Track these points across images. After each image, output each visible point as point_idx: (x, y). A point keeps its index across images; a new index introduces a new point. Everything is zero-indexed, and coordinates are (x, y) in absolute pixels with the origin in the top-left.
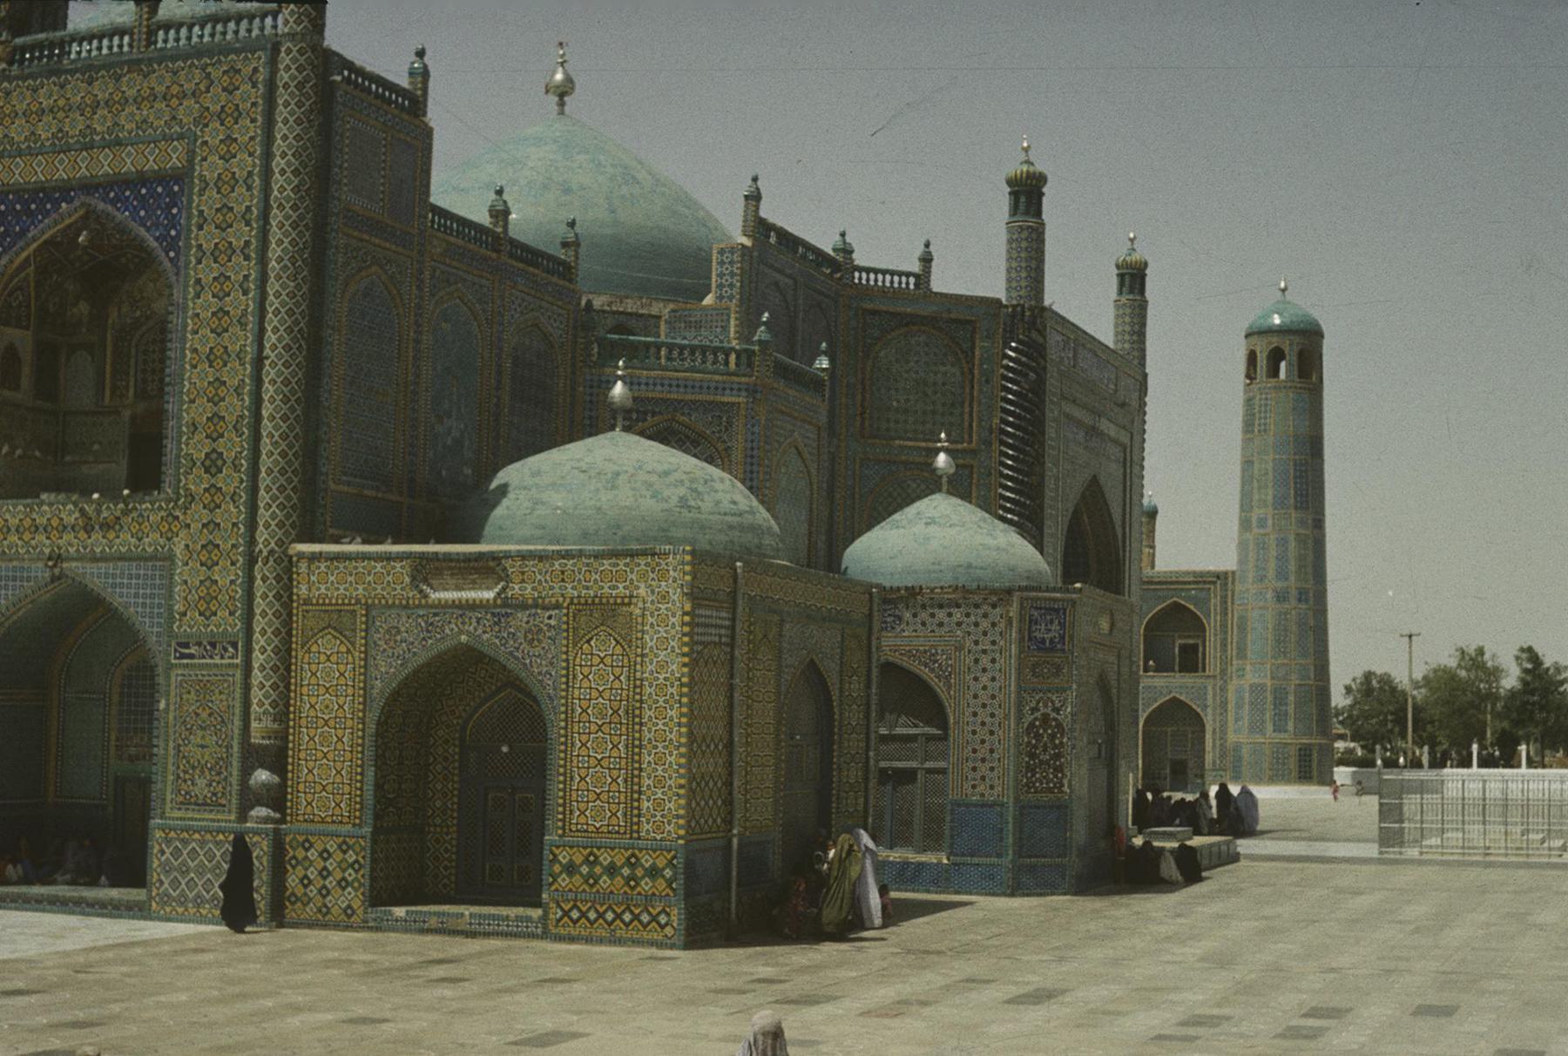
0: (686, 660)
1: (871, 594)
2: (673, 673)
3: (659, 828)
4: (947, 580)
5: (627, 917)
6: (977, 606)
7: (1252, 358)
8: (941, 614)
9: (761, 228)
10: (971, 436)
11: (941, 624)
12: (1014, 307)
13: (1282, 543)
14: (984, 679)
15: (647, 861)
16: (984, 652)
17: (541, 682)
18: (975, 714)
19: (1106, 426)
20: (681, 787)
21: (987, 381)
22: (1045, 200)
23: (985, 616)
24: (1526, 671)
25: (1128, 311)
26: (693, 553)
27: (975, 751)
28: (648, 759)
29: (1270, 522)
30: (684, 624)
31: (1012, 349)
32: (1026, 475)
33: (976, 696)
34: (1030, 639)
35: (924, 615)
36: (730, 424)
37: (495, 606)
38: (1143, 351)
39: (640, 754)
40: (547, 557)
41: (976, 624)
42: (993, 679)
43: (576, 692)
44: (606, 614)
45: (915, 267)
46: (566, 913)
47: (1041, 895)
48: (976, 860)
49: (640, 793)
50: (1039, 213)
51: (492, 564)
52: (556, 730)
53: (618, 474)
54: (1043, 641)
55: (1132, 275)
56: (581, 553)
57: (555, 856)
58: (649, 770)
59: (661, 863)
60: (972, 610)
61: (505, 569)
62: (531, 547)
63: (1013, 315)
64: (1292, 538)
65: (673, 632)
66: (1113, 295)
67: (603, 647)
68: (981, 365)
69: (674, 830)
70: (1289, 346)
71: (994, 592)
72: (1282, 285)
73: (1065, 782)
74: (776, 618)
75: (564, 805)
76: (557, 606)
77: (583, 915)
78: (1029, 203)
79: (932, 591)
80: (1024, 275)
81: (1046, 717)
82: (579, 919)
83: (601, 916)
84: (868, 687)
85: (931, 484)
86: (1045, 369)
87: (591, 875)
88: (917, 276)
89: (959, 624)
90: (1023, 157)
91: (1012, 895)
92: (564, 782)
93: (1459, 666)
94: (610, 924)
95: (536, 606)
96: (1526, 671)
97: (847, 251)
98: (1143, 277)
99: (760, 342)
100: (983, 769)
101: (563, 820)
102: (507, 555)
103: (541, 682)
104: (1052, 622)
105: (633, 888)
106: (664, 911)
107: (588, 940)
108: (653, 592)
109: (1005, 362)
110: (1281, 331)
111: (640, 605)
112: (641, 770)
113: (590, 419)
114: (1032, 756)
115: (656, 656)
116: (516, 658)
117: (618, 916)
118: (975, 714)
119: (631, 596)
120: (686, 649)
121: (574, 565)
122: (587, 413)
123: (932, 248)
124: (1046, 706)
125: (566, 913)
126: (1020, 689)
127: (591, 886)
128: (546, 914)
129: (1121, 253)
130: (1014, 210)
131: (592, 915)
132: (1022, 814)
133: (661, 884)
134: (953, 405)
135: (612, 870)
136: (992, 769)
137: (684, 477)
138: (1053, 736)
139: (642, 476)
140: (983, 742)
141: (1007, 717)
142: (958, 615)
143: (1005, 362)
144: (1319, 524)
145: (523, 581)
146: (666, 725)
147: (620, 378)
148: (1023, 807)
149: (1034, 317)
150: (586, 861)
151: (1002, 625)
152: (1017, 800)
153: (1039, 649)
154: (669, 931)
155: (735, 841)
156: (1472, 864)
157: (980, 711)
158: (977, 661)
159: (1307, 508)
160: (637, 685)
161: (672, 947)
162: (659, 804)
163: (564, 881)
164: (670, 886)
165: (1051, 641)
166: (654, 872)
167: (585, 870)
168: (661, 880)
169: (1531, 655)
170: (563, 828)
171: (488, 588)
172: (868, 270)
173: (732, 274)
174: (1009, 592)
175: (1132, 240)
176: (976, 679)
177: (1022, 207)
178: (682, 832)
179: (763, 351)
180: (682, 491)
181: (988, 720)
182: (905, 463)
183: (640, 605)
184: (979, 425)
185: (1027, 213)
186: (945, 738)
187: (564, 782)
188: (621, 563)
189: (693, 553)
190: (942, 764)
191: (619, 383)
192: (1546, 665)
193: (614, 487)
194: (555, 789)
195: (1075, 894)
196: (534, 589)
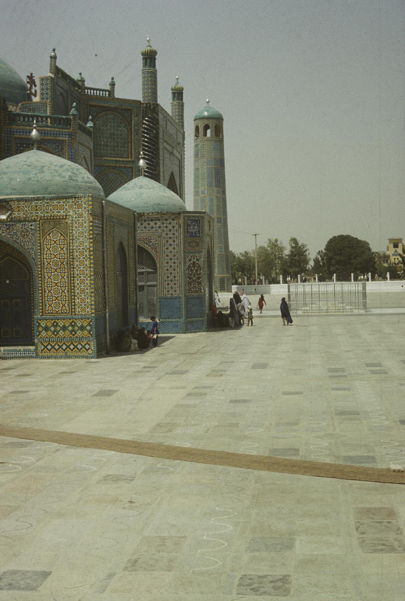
0: (91, 241)
1: (134, 215)
2: (86, 246)
3: (83, 310)
4: (151, 210)
5: (72, 347)
6: (166, 220)
7: (197, 129)
8: (152, 224)
9: (58, 71)
10: (132, 156)
11: (152, 228)
12: (147, 104)
13: (211, 200)
14: (171, 249)
15: (79, 324)
16: (170, 238)
17: (29, 252)
18: (167, 263)
19: (175, 152)
20: (92, 292)
21: (137, 134)
22: (156, 61)
23: (170, 223)
24: (293, 247)
25: (177, 107)
26: (92, 196)
27: (168, 277)
28: (77, 282)
29: (206, 193)
30: (89, 226)
31: (146, 120)
32: (154, 170)
33: (167, 256)
34: (187, 232)
35: (145, 224)
36: (62, 148)
37: (7, 221)
38: (183, 123)
39: (74, 280)
40: (29, 200)
41: (167, 227)
42: (174, 248)
43: (45, 256)
44: (56, 223)
45: (108, 88)
46: (45, 347)
47: (195, 332)
48: (170, 320)
49: (74, 296)
50: (154, 66)
51: (4, 204)
52: (36, 271)
53: (43, 167)
54: (192, 233)
55: (178, 93)
56: (44, 198)
57: (39, 324)
58: (78, 286)
59: (85, 324)
60: (165, 222)
61: (11, 206)
62: (21, 196)
63: (146, 107)
64: (215, 198)
65: (85, 230)
66: (171, 101)
67: (55, 237)
68: (134, 127)
69: (89, 311)
70: (211, 123)
71: (173, 214)
72: (207, 100)
73: (202, 288)
74: (112, 224)
75: (42, 303)
76: (35, 221)
77: (53, 347)
78: (151, 62)
79: (148, 214)
80: (150, 91)
81: (194, 264)
82: (51, 349)
83: (60, 347)
84: (135, 252)
85: (138, 172)
86: (159, 128)
87: (55, 331)
88: (109, 91)
89: (159, 227)
90: (148, 44)
91: (185, 333)
92: (42, 293)
93: (268, 246)
94: (64, 350)
95: (25, 221)
96: (293, 247)
97: (83, 81)
98: (182, 93)
99: (73, 115)
100: (172, 284)
101: (42, 309)
102: (12, 200)
103: (29, 252)
104: (195, 225)
105: (73, 335)
106: (87, 343)
107: (56, 357)
108: (76, 213)
109: (144, 126)
110: (208, 118)
111: (71, 218)
112: (74, 287)
113: (25, 145)
114: (190, 278)
115: (79, 239)
116: (18, 243)
117: (68, 347)
118: (167, 263)
119: (66, 215)
120: (91, 236)
121: (41, 203)
122: (6, 145)
123: (114, 80)
124: (194, 258)
125: (45, 347)
126: (185, 252)
127: (56, 335)
128: (37, 349)
129: (173, 84)
130: (145, 64)
131: (57, 347)
132: (187, 301)
133: (86, 332)
134: (124, 143)
135: (64, 328)
136: (175, 284)
137: (69, 168)
138: (197, 270)
139: (53, 167)
140: (171, 273)
141: (180, 263)
142: (159, 223)
143: (144, 126)
144: (224, 193)
145: (19, 211)
146: (84, 269)
147: (35, 128)
148: (187, 298)
149: (154, 108)
150: (53, 325)
151: (177, 227)
152: (185, 296)
153: (191, 236)
154: (90, 351)
155: (107, 314)
156: (314, 316)
157: (169, 261)
158: (167, 241)
159: (220, 187)
160: (71, 252)
161: (92, 358)
162: (83, 300)
163: (44, 333)
164: (89, 333)
165: (195, 233)
166: (82, 328)
167: (52, 329)
168: (85, 331)
169: (294, 241)
170: (42, 312)
171: (5, 214)
172: (91, 89)
173: (47, 89)
174: (179, 214)
175: (177, 79)
176: (167, 249)
177: (148, 63)
178: (93, 311)
179: (74, 119)
180: (70, 173)
181: (173, 265)
182: (108, 166)
183: (71, 218)
184: (135, 151)
185: (150, 66)
186: (156, 272)
187: (42, 293)
188: (61, 201)
189: (92, 196)
190: (155, 283)
191: (34, 130)
192: (299, 245)
193: (43, 172)
194: (38, 296)
195: (207, 332)
196: (24, 214)
